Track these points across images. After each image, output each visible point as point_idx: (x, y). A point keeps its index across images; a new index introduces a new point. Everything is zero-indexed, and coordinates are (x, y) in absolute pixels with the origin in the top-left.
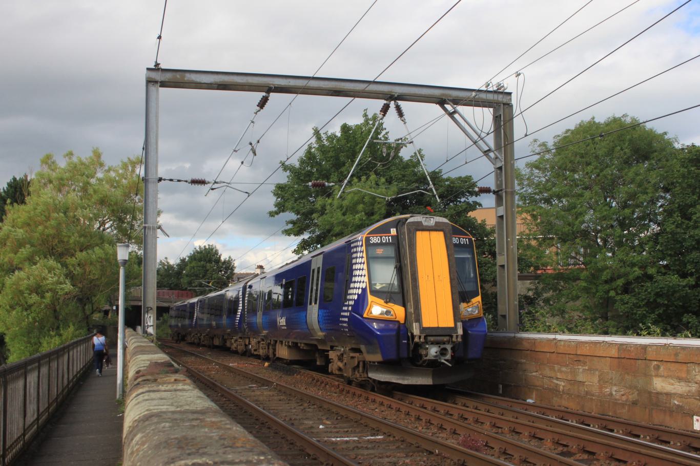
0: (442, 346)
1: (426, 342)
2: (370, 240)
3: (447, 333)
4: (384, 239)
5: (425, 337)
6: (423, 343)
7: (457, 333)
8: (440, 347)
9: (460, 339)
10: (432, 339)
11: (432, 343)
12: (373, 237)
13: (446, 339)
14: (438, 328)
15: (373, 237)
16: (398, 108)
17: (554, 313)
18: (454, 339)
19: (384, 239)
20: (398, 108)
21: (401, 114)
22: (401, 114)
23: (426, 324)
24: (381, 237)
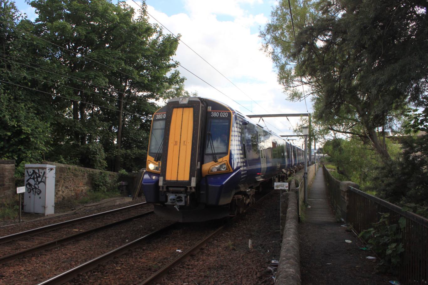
0: (178, 195)
1: (168, 191)
2: (212, 114)
3: (184, 185)
4: (221, 114)
5: (167, 188)
6: (165, 192)
7: (191, 185)
8: (176, 195)
9: (193, 190)
10: (171, 189)
11: (173, 192)
12: (214, 112)
13: (182, 189)
14: (184, 181)
15: (214, 112)
16: (262, 119)
17: (39, 179)
18: (189, 190)
19: (221, 114)
20: (262, 119)
21: (263, 120)
22: (263, 120)
23: (168, 178)
24: (220, 113)
